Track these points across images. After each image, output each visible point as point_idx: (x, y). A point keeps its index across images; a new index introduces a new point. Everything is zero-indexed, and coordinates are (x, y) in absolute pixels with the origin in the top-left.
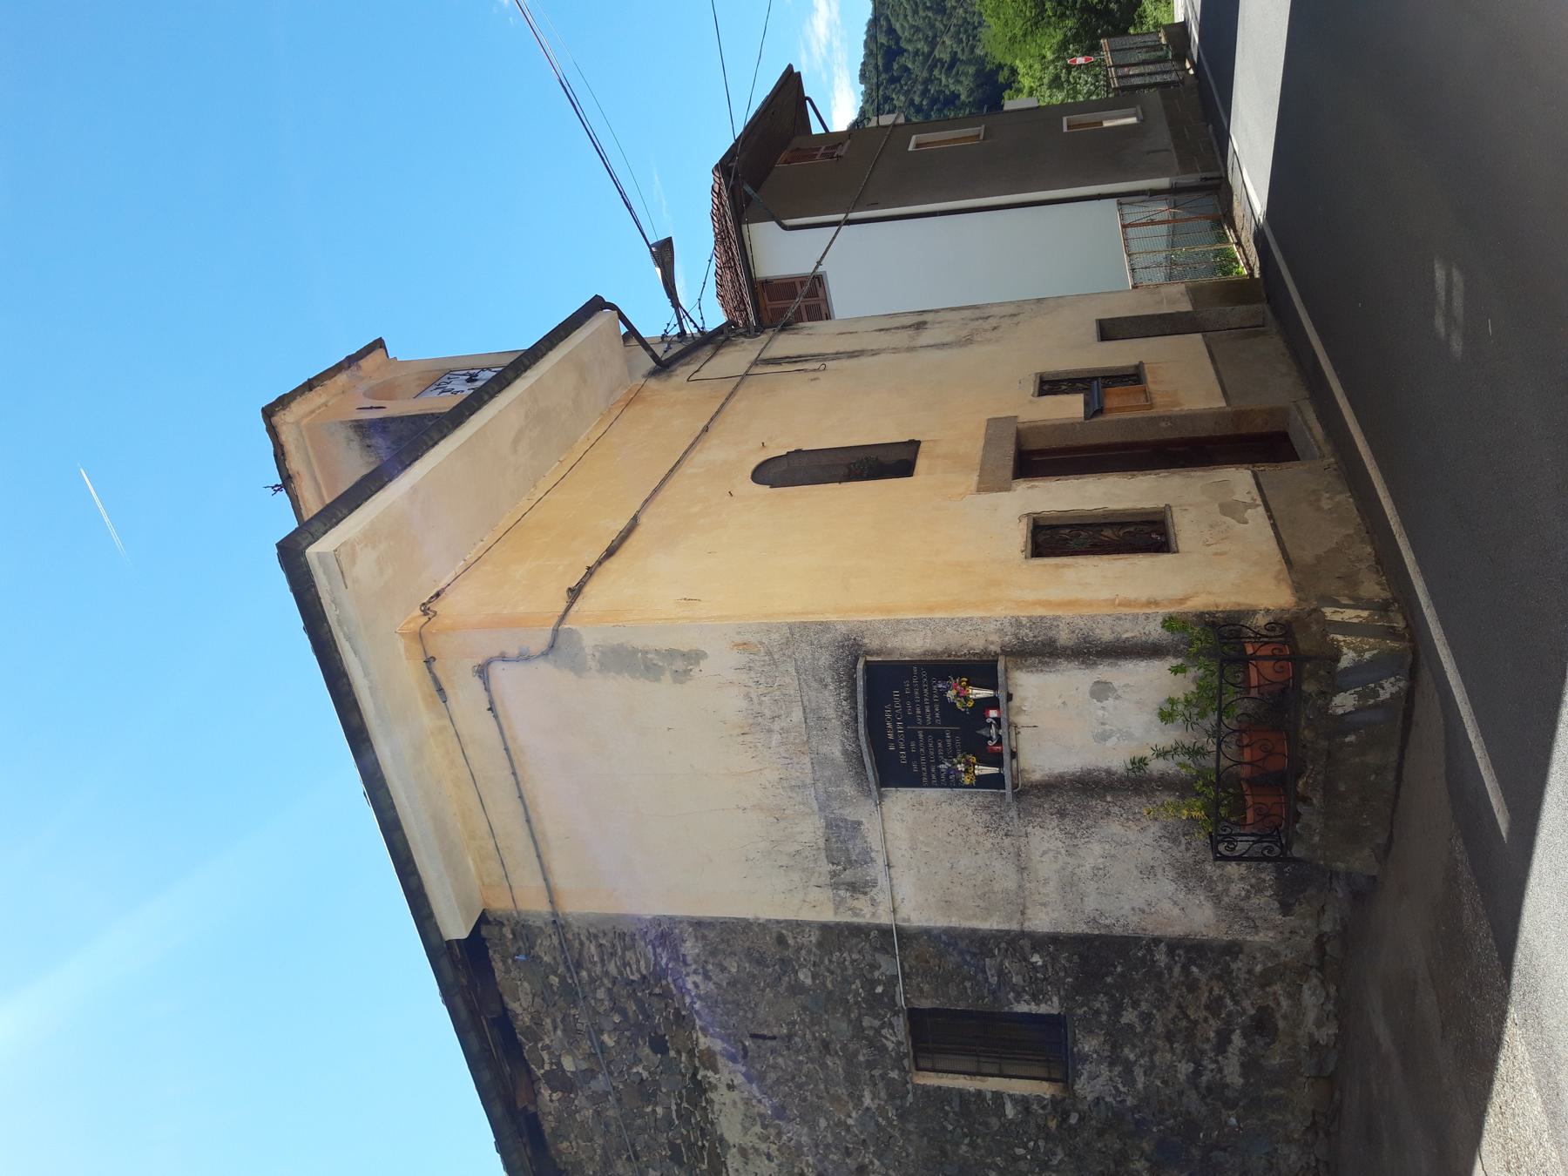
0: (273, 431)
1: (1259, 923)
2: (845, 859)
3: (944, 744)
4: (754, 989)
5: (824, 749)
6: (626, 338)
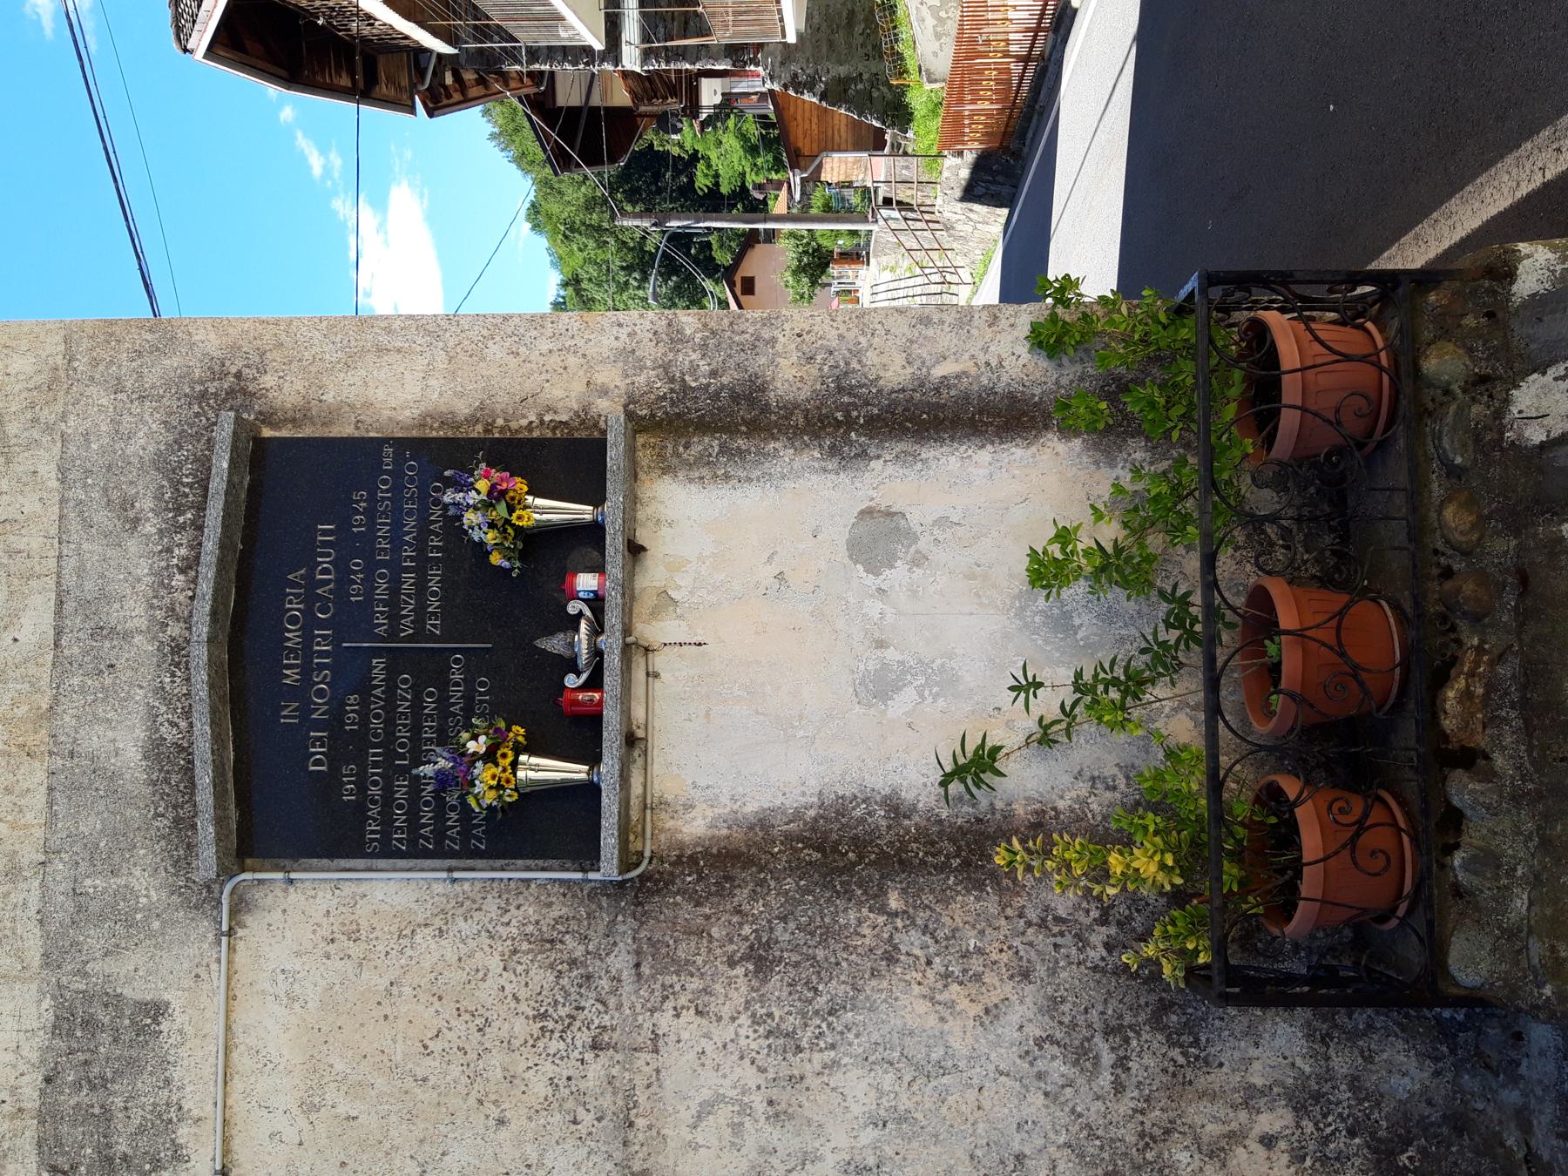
5: (94, 739)
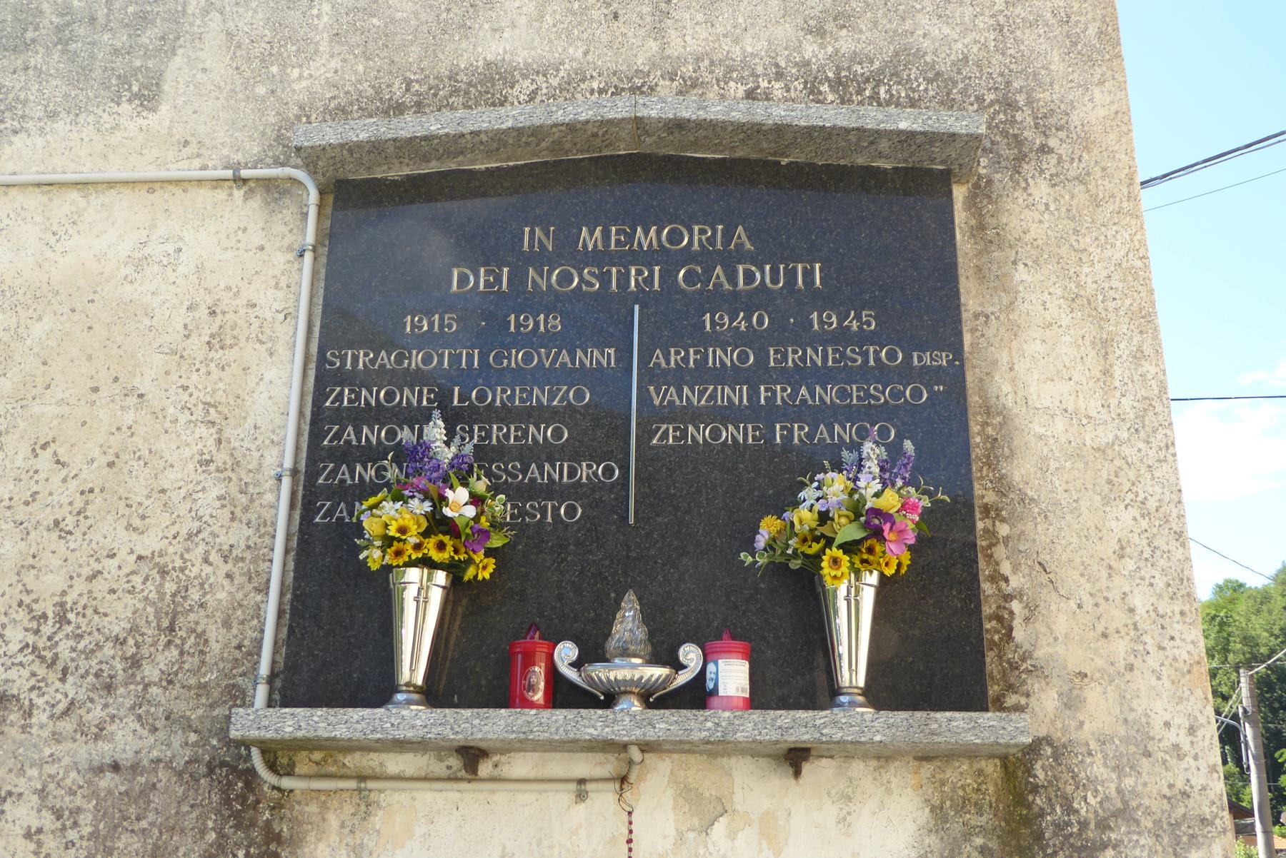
3: (548, 453)
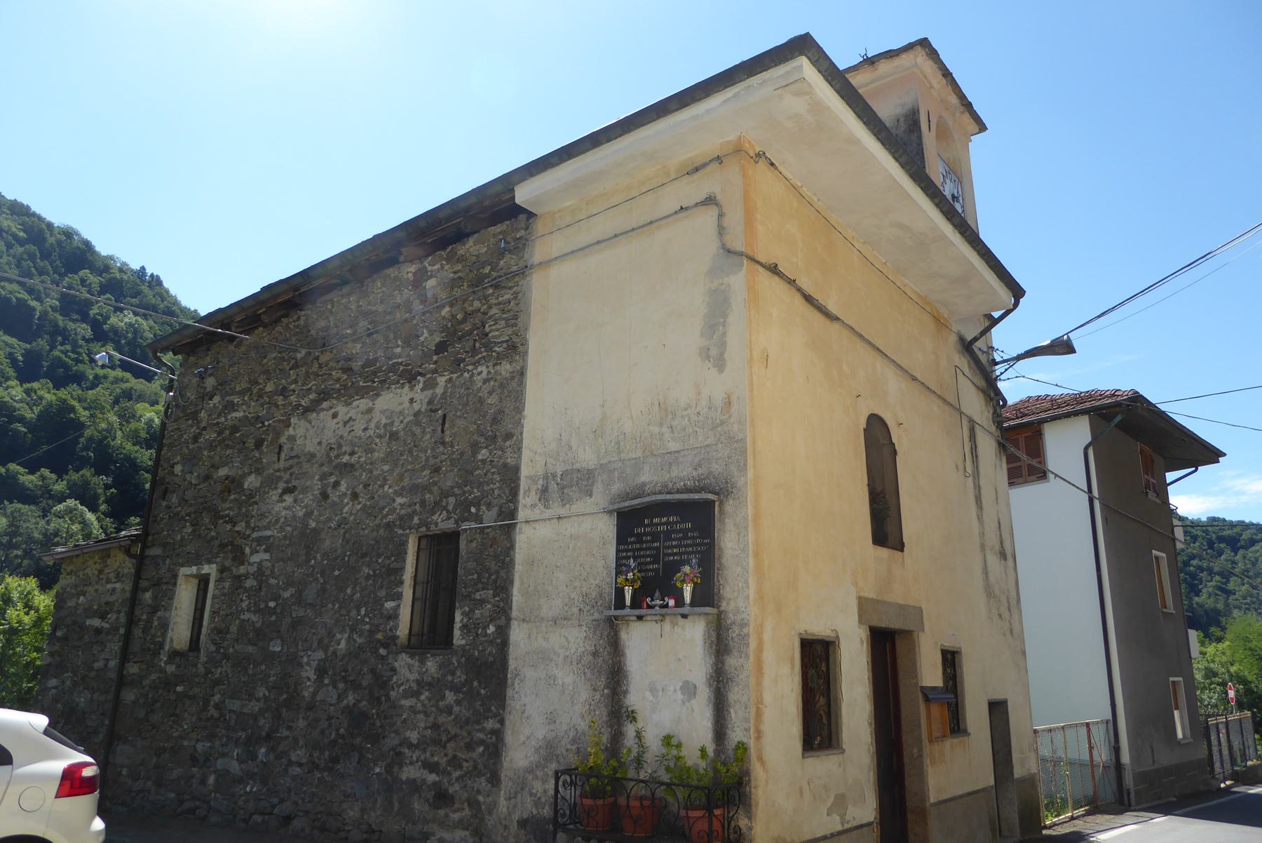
0: (909, 47)
1: (513, 801)
2: (568, 484)
4: (476, 416)
5: (646, 468)
6: (989, 317)
